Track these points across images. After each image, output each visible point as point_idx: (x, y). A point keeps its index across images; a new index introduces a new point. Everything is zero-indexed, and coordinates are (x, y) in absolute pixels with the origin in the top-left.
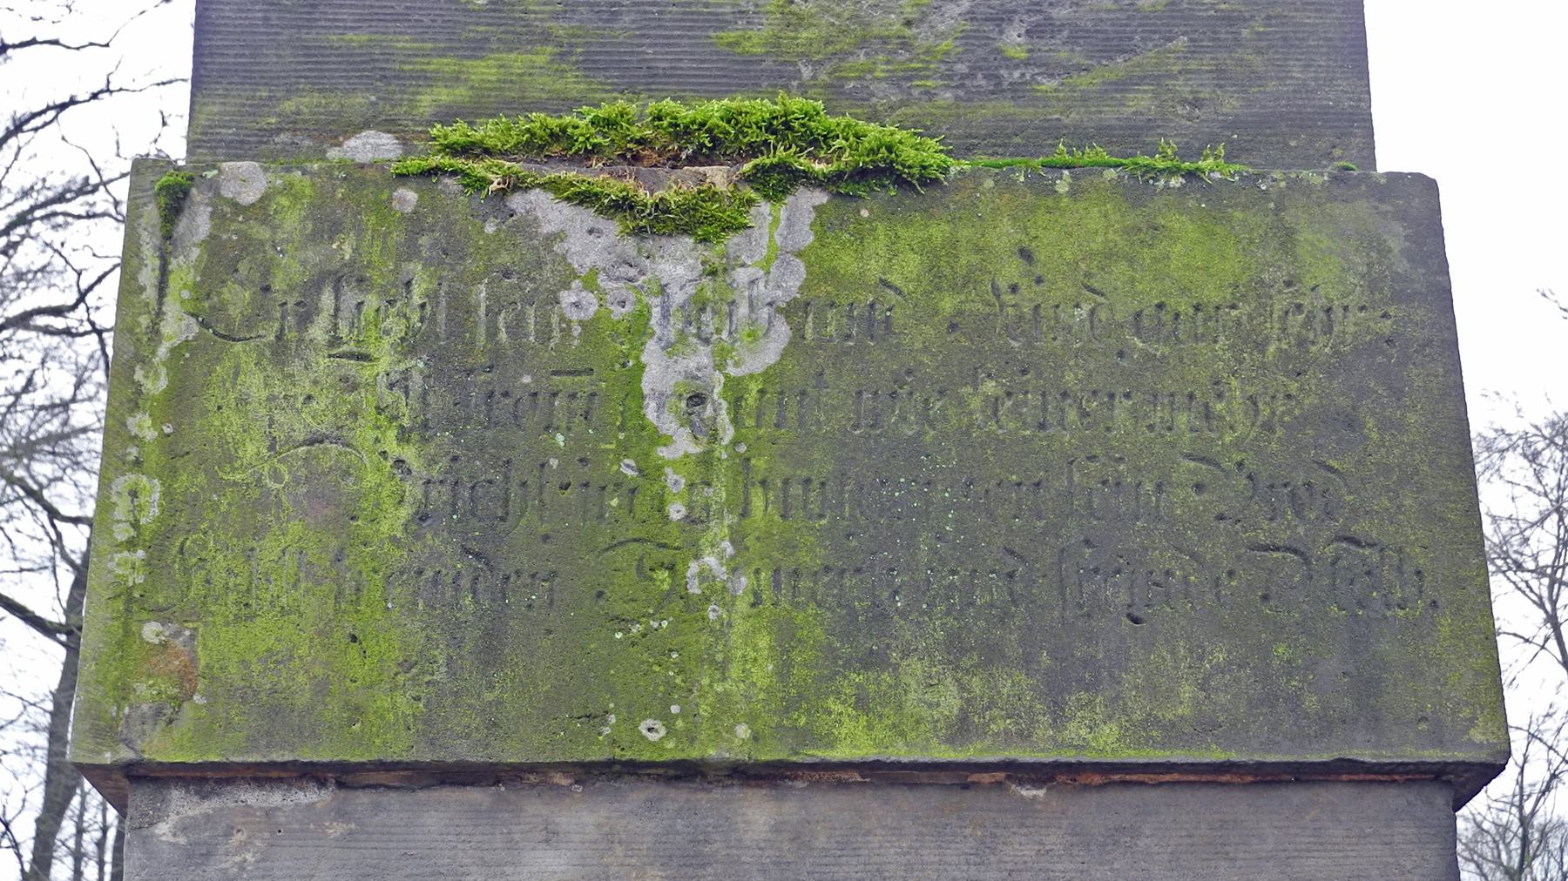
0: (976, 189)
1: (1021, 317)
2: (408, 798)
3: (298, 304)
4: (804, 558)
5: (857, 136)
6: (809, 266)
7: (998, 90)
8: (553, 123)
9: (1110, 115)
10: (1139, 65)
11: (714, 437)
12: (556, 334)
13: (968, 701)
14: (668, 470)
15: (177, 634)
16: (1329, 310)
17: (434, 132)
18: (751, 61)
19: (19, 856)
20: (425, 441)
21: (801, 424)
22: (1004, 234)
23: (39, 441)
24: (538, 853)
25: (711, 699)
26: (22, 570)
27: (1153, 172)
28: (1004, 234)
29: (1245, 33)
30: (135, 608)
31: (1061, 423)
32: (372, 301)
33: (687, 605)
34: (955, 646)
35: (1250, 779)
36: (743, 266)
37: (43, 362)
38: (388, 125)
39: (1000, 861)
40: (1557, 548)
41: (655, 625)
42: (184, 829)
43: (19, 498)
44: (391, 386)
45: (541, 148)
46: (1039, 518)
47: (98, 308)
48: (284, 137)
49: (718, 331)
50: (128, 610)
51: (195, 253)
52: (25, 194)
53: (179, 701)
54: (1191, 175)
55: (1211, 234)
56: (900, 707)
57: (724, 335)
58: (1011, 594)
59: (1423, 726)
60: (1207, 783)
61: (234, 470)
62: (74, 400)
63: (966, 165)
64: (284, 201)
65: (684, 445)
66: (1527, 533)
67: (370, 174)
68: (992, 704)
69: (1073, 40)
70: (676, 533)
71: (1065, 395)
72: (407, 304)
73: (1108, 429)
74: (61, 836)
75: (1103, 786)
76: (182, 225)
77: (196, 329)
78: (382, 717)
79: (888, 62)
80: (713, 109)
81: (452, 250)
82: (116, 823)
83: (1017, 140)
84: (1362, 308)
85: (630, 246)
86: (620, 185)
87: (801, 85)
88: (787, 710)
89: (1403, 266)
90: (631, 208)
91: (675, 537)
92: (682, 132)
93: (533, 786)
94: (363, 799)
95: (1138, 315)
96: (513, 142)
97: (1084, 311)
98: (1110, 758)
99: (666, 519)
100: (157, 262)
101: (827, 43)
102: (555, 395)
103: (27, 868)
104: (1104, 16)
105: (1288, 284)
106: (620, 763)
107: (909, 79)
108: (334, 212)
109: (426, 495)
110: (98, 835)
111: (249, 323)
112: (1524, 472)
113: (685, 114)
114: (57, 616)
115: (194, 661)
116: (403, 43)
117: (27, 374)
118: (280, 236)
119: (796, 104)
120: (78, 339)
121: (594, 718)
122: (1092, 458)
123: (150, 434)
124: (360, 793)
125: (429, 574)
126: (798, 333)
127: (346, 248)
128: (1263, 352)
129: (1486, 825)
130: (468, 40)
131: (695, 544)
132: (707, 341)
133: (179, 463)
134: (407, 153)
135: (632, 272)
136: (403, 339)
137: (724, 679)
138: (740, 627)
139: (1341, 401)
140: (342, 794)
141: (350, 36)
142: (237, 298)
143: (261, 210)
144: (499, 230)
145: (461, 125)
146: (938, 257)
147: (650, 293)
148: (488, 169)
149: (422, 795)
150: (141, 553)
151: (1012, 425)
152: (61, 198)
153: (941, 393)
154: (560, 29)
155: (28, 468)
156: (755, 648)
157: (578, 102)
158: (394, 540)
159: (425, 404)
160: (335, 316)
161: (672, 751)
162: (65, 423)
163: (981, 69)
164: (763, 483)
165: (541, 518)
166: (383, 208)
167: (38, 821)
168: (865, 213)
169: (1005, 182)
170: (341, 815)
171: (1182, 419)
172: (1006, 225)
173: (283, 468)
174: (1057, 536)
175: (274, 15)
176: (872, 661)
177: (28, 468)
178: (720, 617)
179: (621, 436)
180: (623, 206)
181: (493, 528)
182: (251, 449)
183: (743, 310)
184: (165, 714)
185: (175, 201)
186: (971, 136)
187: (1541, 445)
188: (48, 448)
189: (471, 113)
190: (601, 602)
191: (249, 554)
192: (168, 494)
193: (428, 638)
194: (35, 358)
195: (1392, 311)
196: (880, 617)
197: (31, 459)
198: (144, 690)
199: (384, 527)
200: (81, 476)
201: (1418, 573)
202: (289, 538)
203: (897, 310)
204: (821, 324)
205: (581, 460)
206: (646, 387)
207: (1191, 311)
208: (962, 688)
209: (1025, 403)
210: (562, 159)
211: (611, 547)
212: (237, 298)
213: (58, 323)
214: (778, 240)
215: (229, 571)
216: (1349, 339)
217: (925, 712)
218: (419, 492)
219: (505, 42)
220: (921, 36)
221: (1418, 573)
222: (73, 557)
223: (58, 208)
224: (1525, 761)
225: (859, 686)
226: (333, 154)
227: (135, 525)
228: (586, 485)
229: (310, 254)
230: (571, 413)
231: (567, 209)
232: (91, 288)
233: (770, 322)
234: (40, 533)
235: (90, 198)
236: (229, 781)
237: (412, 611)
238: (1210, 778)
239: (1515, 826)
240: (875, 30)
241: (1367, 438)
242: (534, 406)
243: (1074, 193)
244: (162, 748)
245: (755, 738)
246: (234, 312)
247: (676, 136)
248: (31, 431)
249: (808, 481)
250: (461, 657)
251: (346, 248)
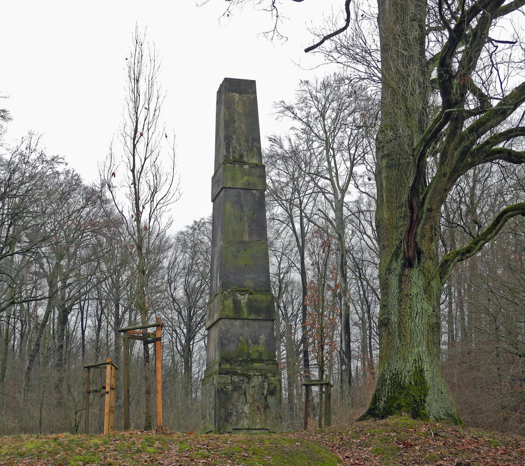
81: (233, 296)
82: (267, 387)
224: (281, 260)
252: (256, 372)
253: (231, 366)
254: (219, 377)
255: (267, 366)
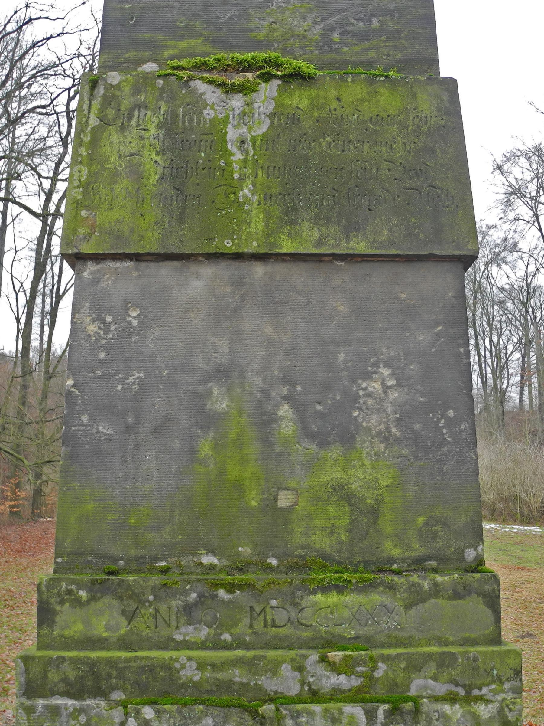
0: (324, 80)
1: (337, 118)
2: (156, 264)
3: (128, 114)
4: (273, 190)
5: (290, 64)
6: (276, 102)
7: (331, 51)
8: (203, 60)
9: (363, 58)
10: (372, 44)
11: (248, 154)
12: (202, 123)
13: (321, 235)
14: (234, 164)
15: (91, 214)
16: (426, 117)
17: (168, 63)
18: (260, 42)
19: (26, 295)
20: (163, 155)
21: (273, 150)
22: (332, 93)
23: (36, 151)
24: (194, 282)
25: (246, 233)
26: (29, 195)
27: (375, 76)
28: (332, 93)
29: (402, 35)
30: (79, 206)
31: (349, 150)
32: (149, 113)
33: (239, 206)
34: (317, 218)
35: (404, 260)
36: (257, 102)
37: (38, 125)
38: (155, 61)
39: (331, 285)
40: (537, 190)
41: (229, 211)
42: (91, 274)
43: (29, 170)
44: (154, 138)
45: (199, 67)
46: (342, 179)
47: (57, 106)
48: (125, 65)
49: (249, 122)
50: (77, 207)
51: (99, 99)
52: (36, 67)
53: (91, 234)
54: (386, 77)
55: (392, 94)
56: (301, 236)
57: (251, 123)
58: (334, 202)
59: (454, 244)
60: (392, 261)
61: (108, 164)
62: (48, 137)
63: (322, 73)
64: (125, 84)
65: (238, 156)
66: (527, 185)
67: (150, 75)
68: (328, 236)
69: (353, 36)
70: (236, 183)
71: (350, 142)
72: (159, 114)
73: (363, 152)
74: (39, 288)
75: (361, 262)
76: (96, 91)
77: (99, 122)
78: (149, 239)
79: (299, 42)
80: (249, 56)
81: (172, 98)
83: (337, 65)
84: (436, 117)
85: (224, 96)
86: (221, 78)
87: (274, 49)
88: (268, 237)
89: (447, 105)
90: (224, 85)
91: (236, 184)
92: (240, 63)
93: (193, 261)
94: (143, 265)
95: (371, 118)
96: (191, 66)
97: (355, 117)
98: (362, 253)
99: (233, 178)
100: (88, 102)
101: (282, 36)
102: (201, 141)
103: (28, 299)
104: (362, 29)
105: (415, 109)
106: (218, 253)
107: (305, 47)
108: (139, 87)
109: (163, 171)
110: (51, 287)
111: (114, 120)
112: (526, 164)
113: (241, 57)
114: (39, 211)
115: (95, 222)
116: (160, 37)
117: (33, 128)
118: (124, 94)
119: (273, 54)
120: (50, 116)
121: (211, 239)
122: (358, 161)
123: (85, 154)
124: (142, 263)
125: (164, 195)
126: (272, 123)
127: (142, 97)
128: (407, 129)
129: (515, 287)
130: (179, 36)
131: (242, 186)
132: (246, 125)
133: (93, 162)
134: (160, 69)
135: (225, 104)
136: (158, 124)
137: (249, 228)
138: (254, 212)
139: (430, 145)
140: (137, 263)
141: (145, 35)
142: (111, 112)
143: (118, 87)
144: (186, 92)
145: (176, 61)
146: (313, 100)
147: (229, 110)
148: (183, 74)
149: (161, 263)
150: (81, 189)
151: (334, 151)
152: (46, 69)
153: (314, 141)
154: (205, 32)
155: (32, 160)
156: (259, 218)
157: (210, 54)
158: (154, 185)
159: (164, 144)
160: (139, 118)
161: (234, 250)
162: (44, 145)
163: (326, 44)
164: (262, 167)
165: (197, 178)
166: (153, 85)
167: (32, 282)
168: (292, 87)
169: (333, 78)
170: (137, 269)
171: (384, 149)
172: (333, 91)
173: (122, 163)
174: (348, 184)
175: (124, 29)
176: (293, 222)
177: (32, 160)
178: (248, 209)
179: (221, 153)
180: (222, 85)
181: (183, 181)
182: (113, 158)
183: (256, 115)
184: (87, 238)
185: (94, 84)
186: (323, 64)
187: (531, 155)
188: (39, 153)
189: (179, 57)
190: (214, 204)
191: (112, 189)
192: (89, 172)
193: (163, 215)
194: (36, 123)
195: (444, 118)
196: (295, 209)
197: (33, 157)
198: (81, 231)
199: (151, 181)
200: (49, 163)
201: (453, 197)
202: (123, 185)
203: (301, 116)
204: (279, 119)
205: (209, 161)
206: (228, 138)
207: (387, 117)
208: (320, 231)
209: (338, 144)
210: (205, 70)
211: (217, 187)
212: (111, 112)
213: (44, 111)
214: (267, 95)
215: (106, 195)
216: (432, 126)
217: (308, 238)
218: (161, 170)
219: (189, 36)
220: (309, 35)
221: (453, 197)
222: (46, 190)
223: (46, 72)
224: (528, 264)
225: (289, 230)
226: (139, 69)
227: (80, 181)
228: (210, 168)
229: (132, 99)
230: (206, 146)
231: (206, 85)
232: (55, 99)
233: (264, 119)
234: (35, 183)
235: (56, 69)
236: (105, 259)
237: (159, 207)
238: (393, 259)
239: (525, 287)
240: (296, 33)
241: (437, 156)
242: (195, 144)
243: (353, 81)
244: (86, 248)
245: (259, 246)
246: (110, 117)
247: (238, 64)
248: (33, 148)
249: (275, 167)
250: (173, 221)
251: (142, 97)
252: (321, 670)
253: (131, 617)
254: (29, 710)
255: (413, 612)
